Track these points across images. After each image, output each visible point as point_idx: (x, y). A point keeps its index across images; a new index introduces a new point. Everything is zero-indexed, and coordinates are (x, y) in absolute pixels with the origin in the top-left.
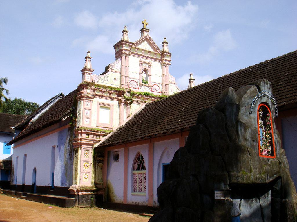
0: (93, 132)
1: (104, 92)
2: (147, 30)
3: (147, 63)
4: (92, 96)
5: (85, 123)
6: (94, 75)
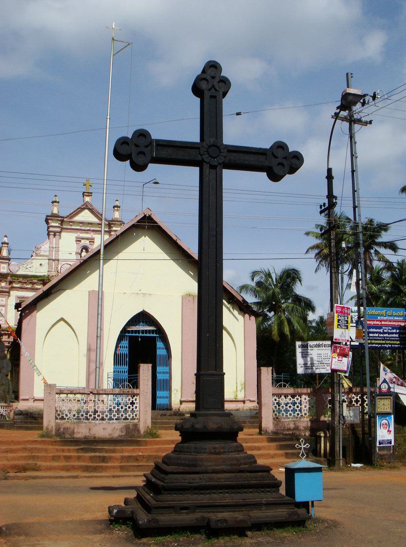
0: (6, 332)
1: (25, 283)
2: (90, 194)
3: (87, 239)
4: (7, 290)
5: (382, 402)
6: (13, 263)
